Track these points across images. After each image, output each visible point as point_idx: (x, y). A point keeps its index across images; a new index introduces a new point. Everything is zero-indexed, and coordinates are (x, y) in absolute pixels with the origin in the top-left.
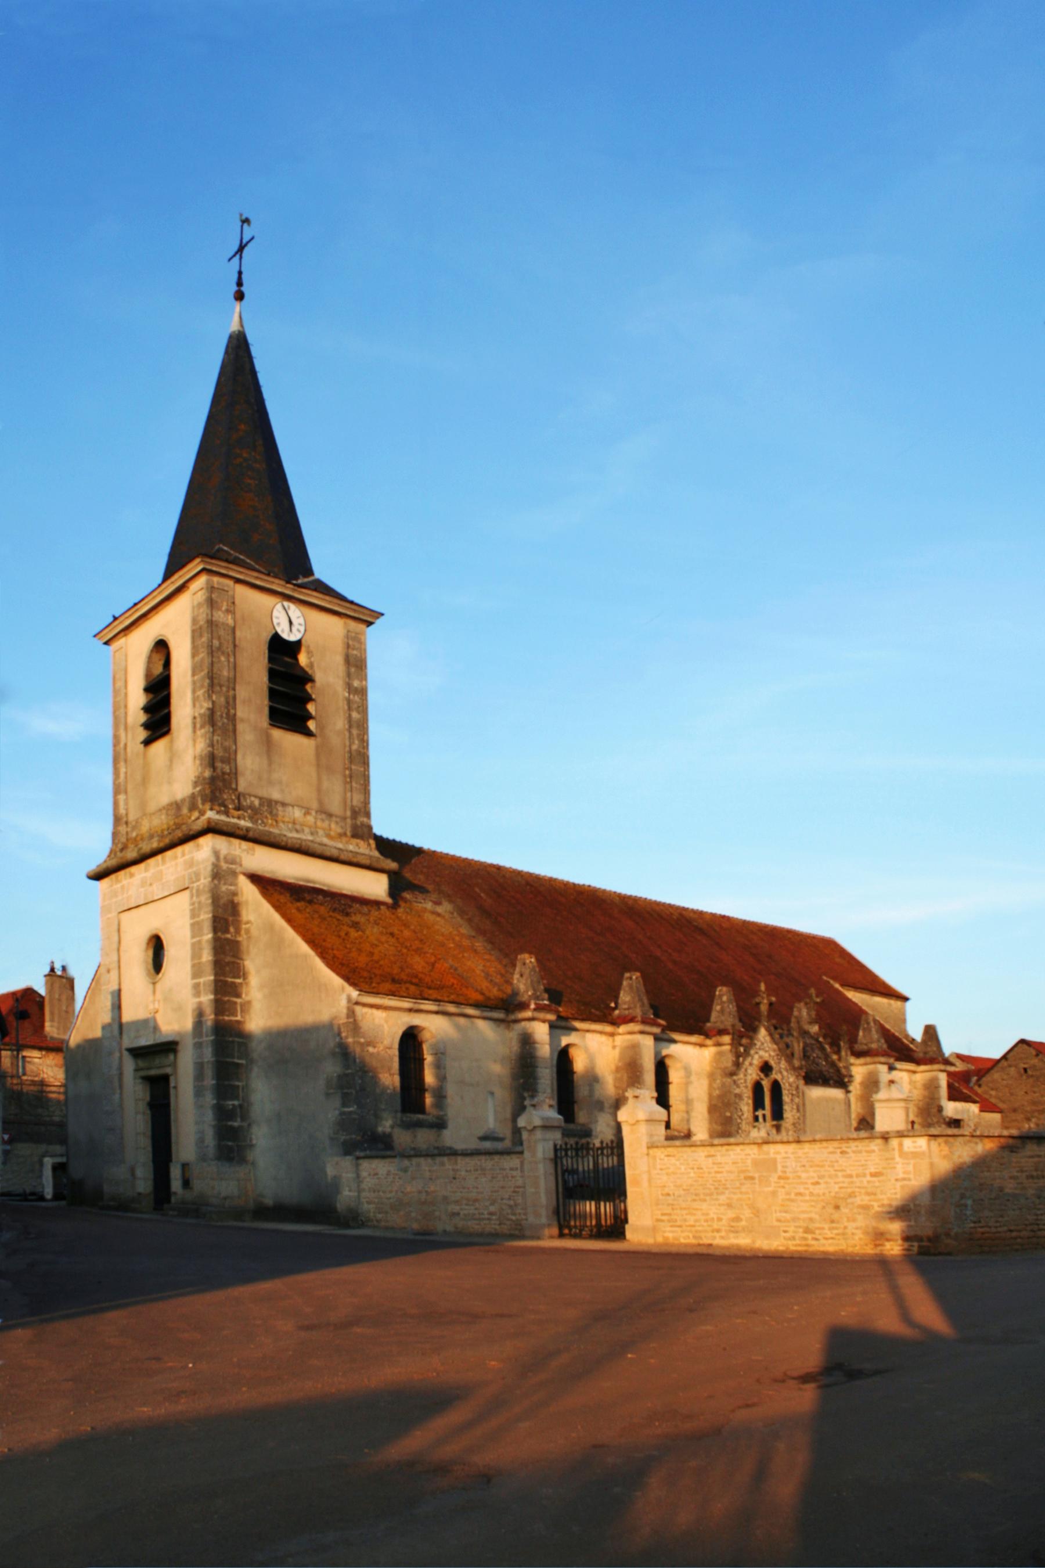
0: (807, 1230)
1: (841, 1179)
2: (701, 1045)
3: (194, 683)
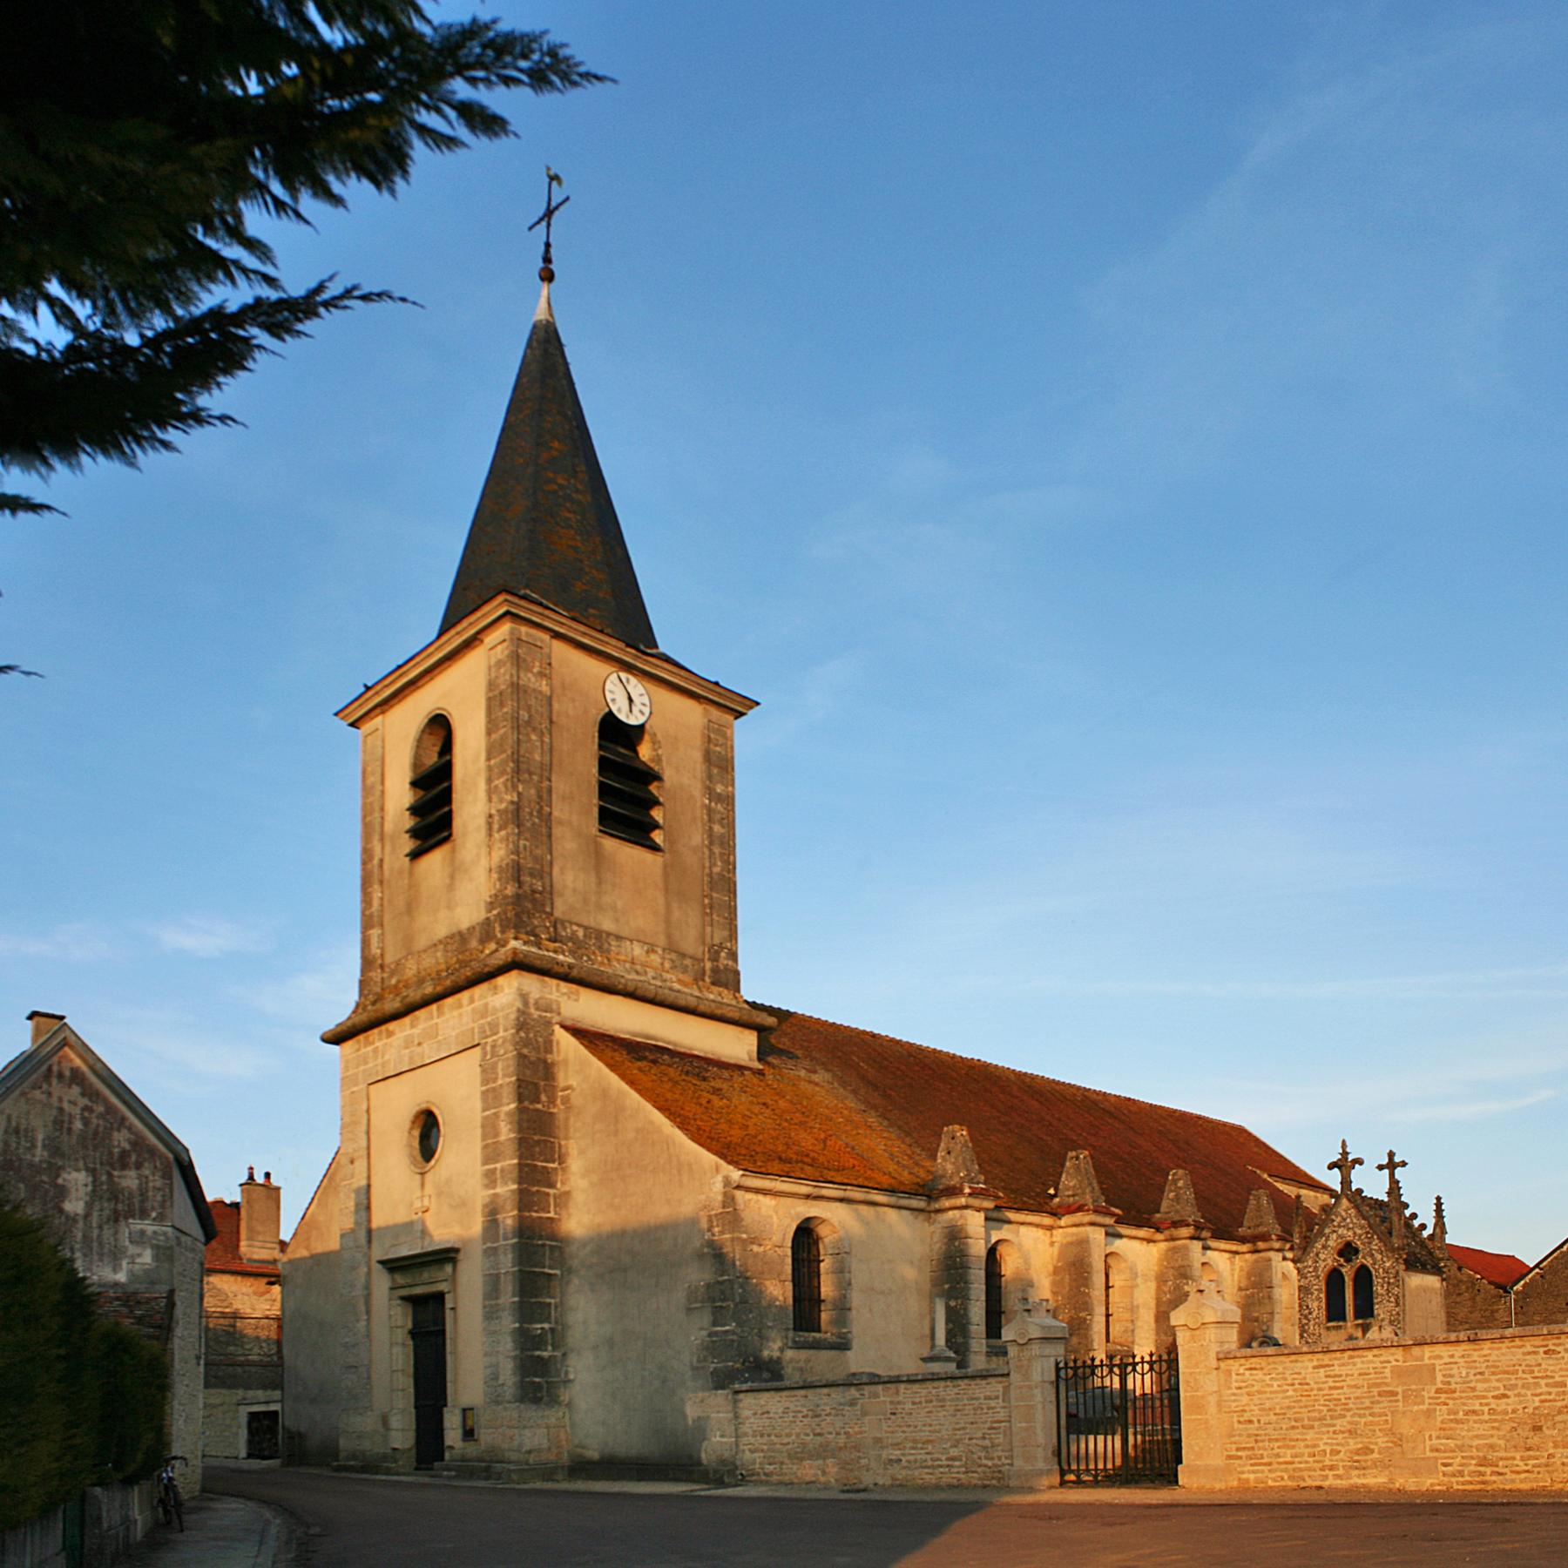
0: (1483, 1462)
1: (1545, 1389)
2: (1149, 1241)
3: (490, 769)
